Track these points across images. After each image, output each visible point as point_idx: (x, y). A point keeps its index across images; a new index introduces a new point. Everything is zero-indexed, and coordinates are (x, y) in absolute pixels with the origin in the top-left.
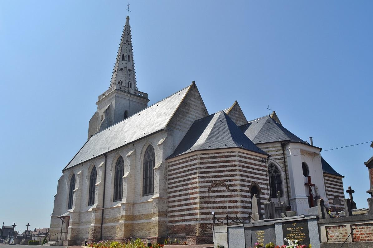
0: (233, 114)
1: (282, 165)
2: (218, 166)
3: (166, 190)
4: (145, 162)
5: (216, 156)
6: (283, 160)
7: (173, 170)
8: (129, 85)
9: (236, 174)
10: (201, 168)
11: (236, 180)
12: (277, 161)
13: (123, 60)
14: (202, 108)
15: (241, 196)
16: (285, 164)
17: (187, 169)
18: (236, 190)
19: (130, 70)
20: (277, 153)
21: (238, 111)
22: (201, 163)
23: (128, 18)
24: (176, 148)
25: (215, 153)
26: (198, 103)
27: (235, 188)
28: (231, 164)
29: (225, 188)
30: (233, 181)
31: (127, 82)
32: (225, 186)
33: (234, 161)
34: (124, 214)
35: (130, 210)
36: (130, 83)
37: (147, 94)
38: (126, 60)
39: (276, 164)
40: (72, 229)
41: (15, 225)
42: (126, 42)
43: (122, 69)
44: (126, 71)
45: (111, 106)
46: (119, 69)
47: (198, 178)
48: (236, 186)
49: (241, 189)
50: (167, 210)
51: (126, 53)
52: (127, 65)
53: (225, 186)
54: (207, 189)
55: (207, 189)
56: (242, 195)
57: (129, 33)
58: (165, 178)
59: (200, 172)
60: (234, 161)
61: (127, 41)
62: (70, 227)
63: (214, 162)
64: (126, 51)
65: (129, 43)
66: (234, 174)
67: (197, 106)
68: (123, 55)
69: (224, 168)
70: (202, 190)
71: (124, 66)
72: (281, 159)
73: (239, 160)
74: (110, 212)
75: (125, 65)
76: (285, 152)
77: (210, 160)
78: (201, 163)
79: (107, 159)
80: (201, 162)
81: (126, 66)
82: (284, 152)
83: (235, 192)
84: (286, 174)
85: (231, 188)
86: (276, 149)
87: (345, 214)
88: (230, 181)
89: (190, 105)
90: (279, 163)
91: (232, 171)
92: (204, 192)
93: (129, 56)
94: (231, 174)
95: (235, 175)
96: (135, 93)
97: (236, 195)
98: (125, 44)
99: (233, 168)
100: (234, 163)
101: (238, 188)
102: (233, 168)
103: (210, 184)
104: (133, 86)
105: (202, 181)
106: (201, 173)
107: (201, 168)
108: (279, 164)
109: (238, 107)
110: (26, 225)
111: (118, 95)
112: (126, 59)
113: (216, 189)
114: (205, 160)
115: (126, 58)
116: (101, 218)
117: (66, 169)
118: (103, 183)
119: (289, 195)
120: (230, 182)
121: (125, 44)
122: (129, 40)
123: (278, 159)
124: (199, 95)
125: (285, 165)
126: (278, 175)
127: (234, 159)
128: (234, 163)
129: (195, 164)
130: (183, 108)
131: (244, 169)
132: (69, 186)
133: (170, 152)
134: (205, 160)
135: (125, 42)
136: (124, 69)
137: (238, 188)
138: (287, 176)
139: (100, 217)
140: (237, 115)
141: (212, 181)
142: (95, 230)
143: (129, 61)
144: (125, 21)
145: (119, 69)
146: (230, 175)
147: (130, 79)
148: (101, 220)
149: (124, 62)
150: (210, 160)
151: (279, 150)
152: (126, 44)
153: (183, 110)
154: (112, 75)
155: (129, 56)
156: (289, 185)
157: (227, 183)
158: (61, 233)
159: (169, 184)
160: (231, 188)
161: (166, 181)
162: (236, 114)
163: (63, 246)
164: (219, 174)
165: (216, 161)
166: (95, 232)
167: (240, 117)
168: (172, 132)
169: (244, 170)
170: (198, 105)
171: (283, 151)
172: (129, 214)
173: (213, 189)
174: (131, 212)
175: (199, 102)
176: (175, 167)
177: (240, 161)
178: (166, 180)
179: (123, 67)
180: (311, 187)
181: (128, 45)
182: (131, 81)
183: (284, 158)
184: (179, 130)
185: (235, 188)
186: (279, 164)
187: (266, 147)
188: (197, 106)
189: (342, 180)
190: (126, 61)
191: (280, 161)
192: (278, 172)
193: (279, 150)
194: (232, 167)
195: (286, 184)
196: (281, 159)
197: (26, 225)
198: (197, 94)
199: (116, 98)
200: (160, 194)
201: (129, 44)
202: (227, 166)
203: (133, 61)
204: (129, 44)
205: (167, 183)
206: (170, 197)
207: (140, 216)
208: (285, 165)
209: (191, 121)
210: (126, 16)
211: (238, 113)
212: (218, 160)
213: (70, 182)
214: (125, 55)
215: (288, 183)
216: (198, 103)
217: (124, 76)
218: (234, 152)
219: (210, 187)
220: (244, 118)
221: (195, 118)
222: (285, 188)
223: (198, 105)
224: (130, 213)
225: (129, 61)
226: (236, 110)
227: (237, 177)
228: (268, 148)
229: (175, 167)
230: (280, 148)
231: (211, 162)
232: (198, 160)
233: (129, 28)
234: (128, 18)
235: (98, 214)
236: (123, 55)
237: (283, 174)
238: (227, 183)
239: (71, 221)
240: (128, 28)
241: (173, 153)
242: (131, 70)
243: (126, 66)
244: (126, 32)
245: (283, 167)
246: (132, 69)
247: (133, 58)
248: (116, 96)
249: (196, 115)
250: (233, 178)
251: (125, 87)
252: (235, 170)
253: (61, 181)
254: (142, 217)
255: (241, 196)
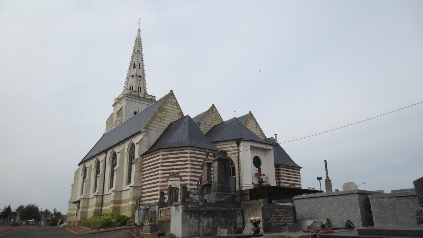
0: (209, 115)
1: (236, 159)
2: (175, 161)
3: (140, 180)
4: (130, 157)
5: (174, 153)
6: (237, 155)
7: (146, 164)
8: (139, 89)
9: (188, 167)
10: (162, 163)
11: (187, 172)
12: (233, 156)
13: (134, 67)
14: (178, 112)
15: (190, 184)
16: (238, 158)
17: (153, 163)
18: (186, 180)
19: (140, 77)
20: (233, 149)
21: (214, 113)
22: (163, 159)
23: (139, 31)
24: (151, 146)
25: (173, 151)
26: (174, 108)
27: (186, 178)
28: (185, 159)
29: (178, 179)
30: (185, 173)
31: (137, 87)
32: (179, 176)
33: (186, 157)
34: (113, 199)
35: (118, 196)
36: (140, 87)
37: (155, 97)
38: (136, 68)
39: (232, 158)
40: (82, 212)
41: (56, 209)
42: (137, 51)
43: (133, 76)
44: (136, 77)
45: (122, 108)
46: (131, 76)
47: (159, 170)
48: (187, 177)
49: (190, 179)
50: (140, 196)
51: (137, 61)
52: (137, 72)
53: (179, 176)
54: (165, 179)
55: (165, 179)
56: (191, 184)
57: (140, 44)
58: (139, 170)
59: (161, 166)
60: (186, 157)
61: (138, 51)
62: (80, 210)
63: (172, 157)
64: (137, 60)
65: (139, 52)
66: (186, 167)
67: (173, 111)
68: (134, 64)
69: (179, 162)
70: (162, 180)
71: (135, 73)
72: (235, 154)
73: (191, 156)
74: (107, 198)
75: (136, 72)
76: (239, 148)
77: (169, 156)
78: (163, 159)
79: (107, 155)
80: (162, 158)
81: (137, 73)
82: (238, 148)
83: (186, 181)
84: (239, 167)
85: (183, 178)
86: (233, 146)
87: (328, 199)
88: (183, 172)
89: (167, 110)
90: (234, 157)
91: (185, 164)
92: (164, 182)
93: (139, 64)
94: (184, 168)
95: (187, 168)
96: (144, 96)
97: (186, 184)
98: (136, 53)
99: (186, 162)
100: (187, 159)
101: (188, 178)
102: (186, 162)
103: (168, 175)
104: (142, 90)
105: (162, 173)
106: (162, 166)
107: (162, 163)
108: (234, 158)
109: (214, 109)
110: (54, 210)
111: (128, 98)
112: (136, 67)
113: (172, 179)
114: (166, 157)
115: (137, 66)
116: (101, 202)
117: (82, 161)
118: (103, 174)
119: (240, 183)
120: (183, 174)
121: (136, 53)
122: (140, 50)
123: (234, 154)
124: (176, 101)
125: (238, 159)
126: (233, 166)
127: (187, 156)
128: (187, 159)
129: (158, 160)
130: (159, 113)
131: (195, 163)
132: (83, 176)
133: (145, 149)
134: (166, 157)
135: (136, 51)
136: (135, 76)
137: (188, 178)
138: (240, 168)
139: (100, 202)
140: (213, 116)
141: (170, 173)
142: (95, 212)
143: (139, 68)
144: (136, 32)
145: (130, 76)
146: (183, 168)
147: (140, 84)
148: (101, 204)
149: (135, 70)
150: (169, 156)
151: (235, 147)
152: (137, 53)
153: (160, 114)
154: (125, 81)
155: (139, 64)
156: (240, 175)
157: (181, 174)
158: (76, 215)
159: (143, 175)
160: (183, 178)
161: (140, 173)
162: (212, 115)
163: (56, 227)
164: (175, 167)
165: (173, 157)
166: (96, 214)
167: (216, 117)
168: (148, 133)
169: (195, 164)
170: (174, 110)
171: (238, 147)
172: (117, 199)
173: (170, 179)
174: (119, 197)
175: (176, 107)
176: (147, 162)
177: (191, 157)
178: (141, 172)
179: (134, 74)
180: (260, 177)
181: (139, 54)
182: (140, 86)
183: (238, 153)
184: (151, 130)
185: (186, 178)
186: (234, 158)
187: (225, 144)
188: (173, 111)
189: (300, 171)
190: (137, 68)
191: (235, 155)
192: (233, 165)
193: (235, 147)
194: (185, 162)
195: (238, 175)
196: (235, 154)
197: (54, 210)
198: (174, 101)
199: (126, 101)
200: (134, 183)
201: (140, 54)
202: (181, 161)
203: (143, 68)
204: (140, 54)
205: (141, 174)
206: (143, 186)
207: (125, 200)
208: (238, 159)
209: (167, 124)
210: (138, 29)
211: (214, 114)
212: (175, 156)
213: (84, 173)
214: (136, 64)
215: (240, 173)
216: (174, 108)
217: (134, 82)
218: (187, 150)
219: (168, 178)
220: (220, 118)
221: (171, 120)
222: (238, 177)
223: (174, 110)
224: (118, 199)
225: (139, 68)
226: (213, 112)
227: (188, 170)
228: (226, 145)
229: (147, 162)
230: (236, 145)
231: (170, 157)
232: (160, 156)
233: (140, 39)
234: (139, 31)
235: (98, 199)
236: (134, 64)
237: (236, 166)
238: (181, 174)
239: (81, 205)
240: (139, 39)
241: (148, 150)
242: (141, 77)
243: (137, 73)
244: (137, 44)
245: (237, 161)
246: (141, 75)
247: (143, 66)
248: (127, 100)
249: (172, 118)
250: (185, 170)
251: (135, 91)
252: (187, 164)
253: (76, 173)
254: (126, 201)
255: (190, 184)
